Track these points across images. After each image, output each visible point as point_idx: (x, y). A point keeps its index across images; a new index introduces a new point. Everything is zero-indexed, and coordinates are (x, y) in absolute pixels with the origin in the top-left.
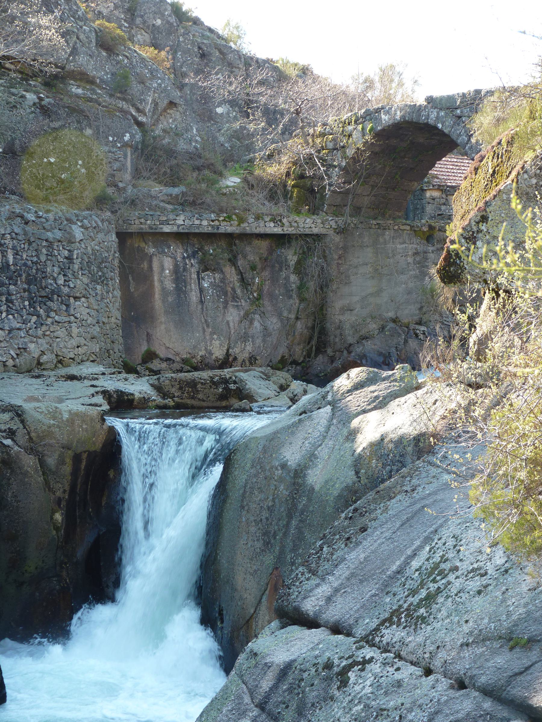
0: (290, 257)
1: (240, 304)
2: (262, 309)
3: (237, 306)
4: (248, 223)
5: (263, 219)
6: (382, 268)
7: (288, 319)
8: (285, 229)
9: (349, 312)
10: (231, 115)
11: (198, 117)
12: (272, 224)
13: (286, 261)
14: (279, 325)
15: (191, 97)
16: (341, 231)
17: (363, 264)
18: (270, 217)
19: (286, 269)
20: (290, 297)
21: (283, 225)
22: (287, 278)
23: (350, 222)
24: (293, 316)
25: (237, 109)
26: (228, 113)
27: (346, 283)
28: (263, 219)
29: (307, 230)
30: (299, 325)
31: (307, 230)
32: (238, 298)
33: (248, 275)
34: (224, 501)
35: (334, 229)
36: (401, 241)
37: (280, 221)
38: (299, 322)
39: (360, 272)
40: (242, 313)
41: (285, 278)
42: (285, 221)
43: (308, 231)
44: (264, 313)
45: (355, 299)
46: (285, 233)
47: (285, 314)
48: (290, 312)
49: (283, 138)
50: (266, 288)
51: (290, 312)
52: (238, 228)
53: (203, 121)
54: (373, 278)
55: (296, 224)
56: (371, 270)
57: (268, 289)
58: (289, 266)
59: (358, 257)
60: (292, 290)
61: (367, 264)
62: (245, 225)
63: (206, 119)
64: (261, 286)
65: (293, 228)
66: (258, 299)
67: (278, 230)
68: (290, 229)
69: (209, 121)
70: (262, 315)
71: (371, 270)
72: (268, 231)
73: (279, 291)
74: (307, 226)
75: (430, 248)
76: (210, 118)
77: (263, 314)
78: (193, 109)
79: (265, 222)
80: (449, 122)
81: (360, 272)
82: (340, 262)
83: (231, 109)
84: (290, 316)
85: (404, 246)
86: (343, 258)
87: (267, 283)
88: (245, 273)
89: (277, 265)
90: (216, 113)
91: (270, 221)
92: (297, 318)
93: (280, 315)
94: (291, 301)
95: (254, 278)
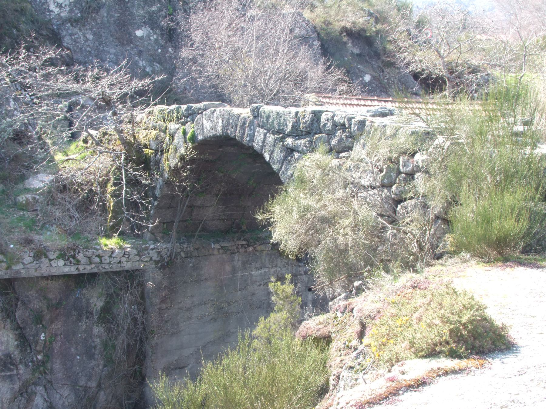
0: (93, 301)
1: (15, 372)
2: (49, 377)
3: (10, 376)
4: (23, 264)
5: (46, 257)
6: (229, 304)
7: (86, 389)
8: (81, 267)
9: (177, 371)
10: (152, 38)
11: (117, 41)
12: (61, 263)
13: (87, 307)
14: (72, 399)
15: (108, 20)
16: (166, 264)
17: (200, 304)
18: (58, 253)
19: (87, 318)
20: (91, 357)
21: (78, 262)
22: (89, 331)
23: (179, 250)
24: (93, 384)
25: (158, 31)
26: (148, 36)
27: (173, 334)
28: (46, 257)
29: (114, 266)
30: (102, 396)
31: (114, 266)
32: (13, 364)
33: (29, 332)
34: (379, 116)
35: (155, 261)
36: (258, 265)
37: (74, 257)
38: (102, 393)
39: (195, 315)
40: (17, 387)
41: (85, 331)
42: (80, 256)
43: (116, 268)
44: (50, 382)
45: (187, 352)
46: (81, 272)
47: (82, 382)
48: (90, 379)
49: (44, 159)
50: (57, 346)
51: (90, 379)
52: (8, 271)
53: (123, 44)
54: (215, 320)
55: (98, 260)
56: (211, 310)
57: (60, 347)
58: (92, 313)
59: (192, 296)
60: (95, 347)
61: (205, 304)
62: (19, 267)
63: (125, 42)
64: (51, 343)
65: (93, 266)
66: (43, 363)
67: (71, 270)
68: (88, 268)
69: (128, 44)
70: (48, 386)
71: (211, 310)
72: (55, 272)
73: (76, 348)
74: (115, 260)
75: (301, 269)
76: (130, 42)
77: (49, 385)
78: (111, 32)
79: (50, 260)
80: (278, 154)
81: (195, 315)
82: (164, 306)
83: (151, 31)
84: (89, 384)
85: (263, 271)
86: (168, 301)
87: (59, 338)
88: (25, 328)
89: (74, 313)
90: (136, 36)
91: (58, 258)
92: (99, 386)
93: (74, 384)
94: (93, 363)
95: (37, 335)
